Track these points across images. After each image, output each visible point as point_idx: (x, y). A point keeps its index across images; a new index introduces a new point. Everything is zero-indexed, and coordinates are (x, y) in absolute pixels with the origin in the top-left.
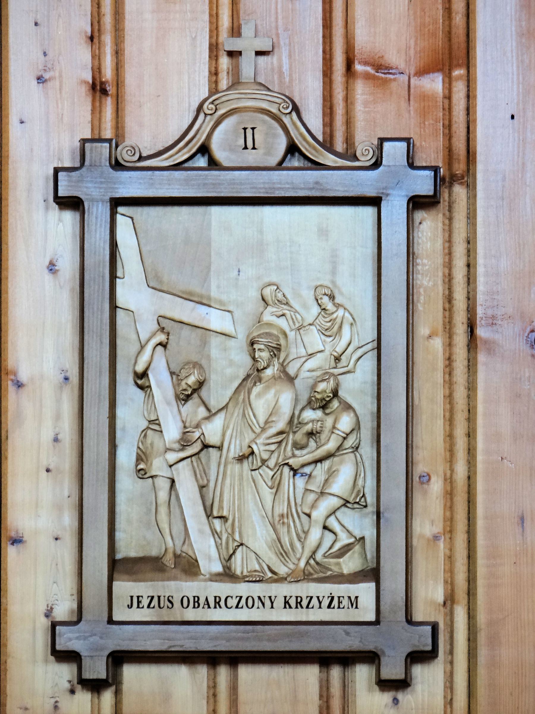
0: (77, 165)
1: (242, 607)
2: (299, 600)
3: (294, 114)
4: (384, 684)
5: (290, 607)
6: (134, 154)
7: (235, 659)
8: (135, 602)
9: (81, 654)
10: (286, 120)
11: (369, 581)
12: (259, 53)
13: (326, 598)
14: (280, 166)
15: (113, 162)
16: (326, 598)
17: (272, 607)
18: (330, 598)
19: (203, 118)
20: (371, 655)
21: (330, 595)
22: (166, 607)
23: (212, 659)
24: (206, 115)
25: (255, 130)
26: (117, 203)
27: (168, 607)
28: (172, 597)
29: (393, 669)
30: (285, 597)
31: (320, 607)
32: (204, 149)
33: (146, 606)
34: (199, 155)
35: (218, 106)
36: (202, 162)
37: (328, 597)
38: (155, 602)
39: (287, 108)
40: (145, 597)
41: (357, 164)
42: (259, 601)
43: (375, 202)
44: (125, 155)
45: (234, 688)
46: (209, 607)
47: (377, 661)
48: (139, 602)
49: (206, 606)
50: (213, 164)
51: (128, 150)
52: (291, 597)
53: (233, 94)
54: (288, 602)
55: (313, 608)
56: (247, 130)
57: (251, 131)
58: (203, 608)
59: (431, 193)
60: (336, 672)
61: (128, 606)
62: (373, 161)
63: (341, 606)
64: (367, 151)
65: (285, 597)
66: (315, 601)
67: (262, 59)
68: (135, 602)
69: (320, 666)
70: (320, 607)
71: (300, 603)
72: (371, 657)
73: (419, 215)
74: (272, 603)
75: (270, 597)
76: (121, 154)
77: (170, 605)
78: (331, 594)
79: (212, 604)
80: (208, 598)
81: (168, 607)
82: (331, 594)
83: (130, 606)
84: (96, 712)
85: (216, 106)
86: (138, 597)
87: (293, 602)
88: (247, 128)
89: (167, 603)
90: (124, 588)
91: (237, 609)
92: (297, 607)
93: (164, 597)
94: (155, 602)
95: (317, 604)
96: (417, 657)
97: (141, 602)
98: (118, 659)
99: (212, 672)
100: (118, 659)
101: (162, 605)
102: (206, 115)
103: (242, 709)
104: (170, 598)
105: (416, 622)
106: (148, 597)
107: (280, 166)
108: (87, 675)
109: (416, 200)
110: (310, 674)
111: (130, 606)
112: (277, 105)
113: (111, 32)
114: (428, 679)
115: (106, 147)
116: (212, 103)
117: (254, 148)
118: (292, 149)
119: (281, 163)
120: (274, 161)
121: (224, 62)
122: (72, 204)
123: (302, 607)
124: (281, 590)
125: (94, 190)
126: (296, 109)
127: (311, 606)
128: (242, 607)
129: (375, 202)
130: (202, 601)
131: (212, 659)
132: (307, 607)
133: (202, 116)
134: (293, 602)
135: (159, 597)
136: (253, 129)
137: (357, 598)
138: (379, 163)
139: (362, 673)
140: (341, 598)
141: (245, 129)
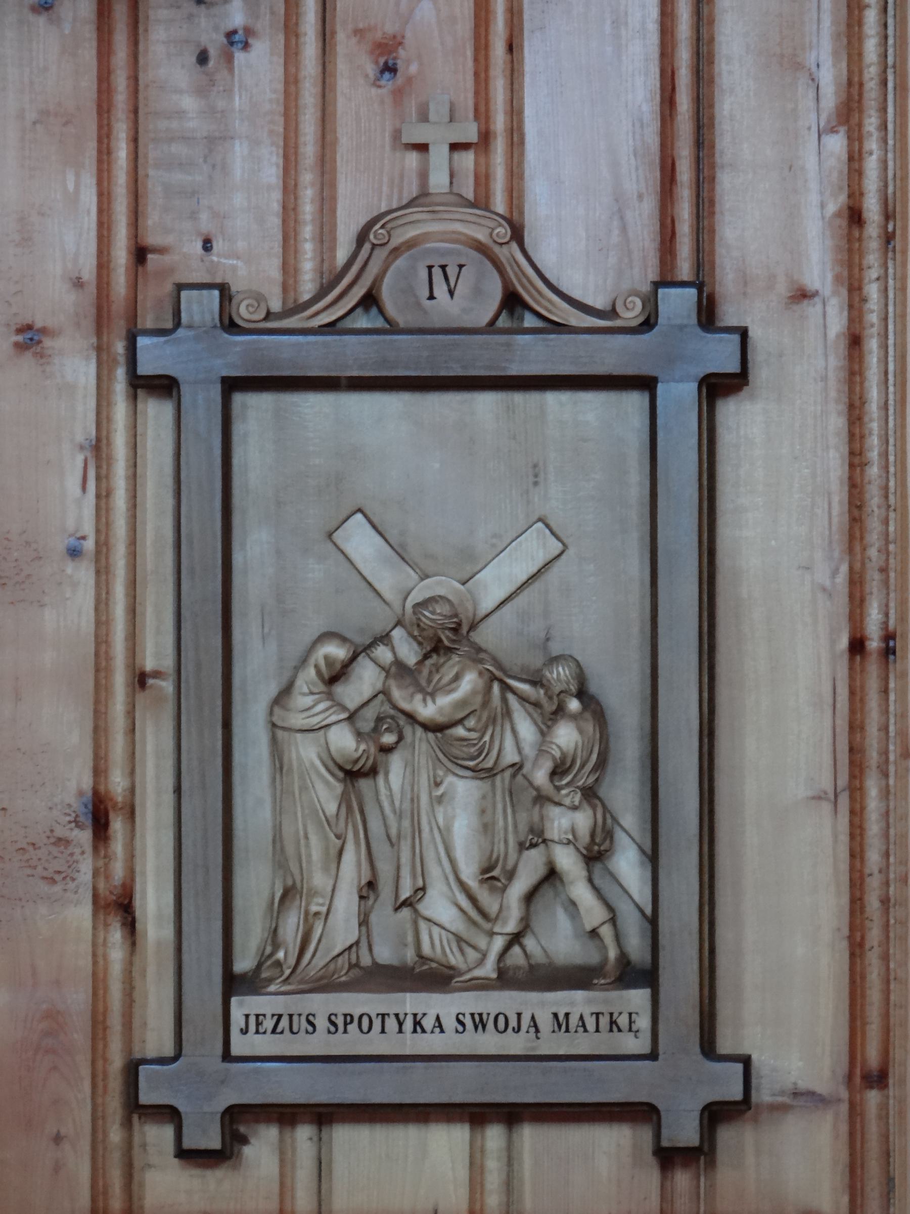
0: (169, 325)
1: (282, 1032)
2: (349, 1018)
3: (514, 246)
5: (424, 1031)
10: (502, 253)
15: (227, 321)
19: (369, 251)
20: (646, 1108)
23: (477, 1115)
25: (464, 269)
26: (232, 386)
29: (685, 1131)
32: (370, 301)
34: (359, 310)
38: (284, 1023)
39: (375, 237)
40: (269, 1016)
41: (618, 323)
43: (646, 384)
45: (322, 1169)
46: (586, 1031)
47: (655, 1118)
48: (258, 1024)
49: (581, 1029)
50: (393, 328)
51: (634, 303)
52: (620, 1013)
54: (615, 1023)
56: (433, 270)
58: (528, 1032)
60: (494, 1136)
61: (242, 1030)
63: (261, 1030)
64: (630, 306)
69: (472, 1129)
72: (641, 1113)
75: (397, 1015)
77: (310, 1029)
79: (591, 1026)
80: (536, 1017)
81: (307, 1032)
83: (244, 1031)
84: (303, 1198)
85: (388, 232)
86: (257, 1016)
88: (433, 266)
93: (300, 1015)
94: (284, 1023)
97: (261, 1023)
98: (238, 1120)
100: (238, 1120)
101: (295, 1029)
103: (340, 1199)
104: (311, 1018)
108: (188, 1143)
113: (879, 237)
116: (382, 227)
124: (321, 1004)
128: (282, 1032)
130: (526, 1021)
133: (367, 247)
134: (428, 1023)
135: (291, 1016)
137: (567, 1015)
140: (261, 1018)
141: (430, 268)
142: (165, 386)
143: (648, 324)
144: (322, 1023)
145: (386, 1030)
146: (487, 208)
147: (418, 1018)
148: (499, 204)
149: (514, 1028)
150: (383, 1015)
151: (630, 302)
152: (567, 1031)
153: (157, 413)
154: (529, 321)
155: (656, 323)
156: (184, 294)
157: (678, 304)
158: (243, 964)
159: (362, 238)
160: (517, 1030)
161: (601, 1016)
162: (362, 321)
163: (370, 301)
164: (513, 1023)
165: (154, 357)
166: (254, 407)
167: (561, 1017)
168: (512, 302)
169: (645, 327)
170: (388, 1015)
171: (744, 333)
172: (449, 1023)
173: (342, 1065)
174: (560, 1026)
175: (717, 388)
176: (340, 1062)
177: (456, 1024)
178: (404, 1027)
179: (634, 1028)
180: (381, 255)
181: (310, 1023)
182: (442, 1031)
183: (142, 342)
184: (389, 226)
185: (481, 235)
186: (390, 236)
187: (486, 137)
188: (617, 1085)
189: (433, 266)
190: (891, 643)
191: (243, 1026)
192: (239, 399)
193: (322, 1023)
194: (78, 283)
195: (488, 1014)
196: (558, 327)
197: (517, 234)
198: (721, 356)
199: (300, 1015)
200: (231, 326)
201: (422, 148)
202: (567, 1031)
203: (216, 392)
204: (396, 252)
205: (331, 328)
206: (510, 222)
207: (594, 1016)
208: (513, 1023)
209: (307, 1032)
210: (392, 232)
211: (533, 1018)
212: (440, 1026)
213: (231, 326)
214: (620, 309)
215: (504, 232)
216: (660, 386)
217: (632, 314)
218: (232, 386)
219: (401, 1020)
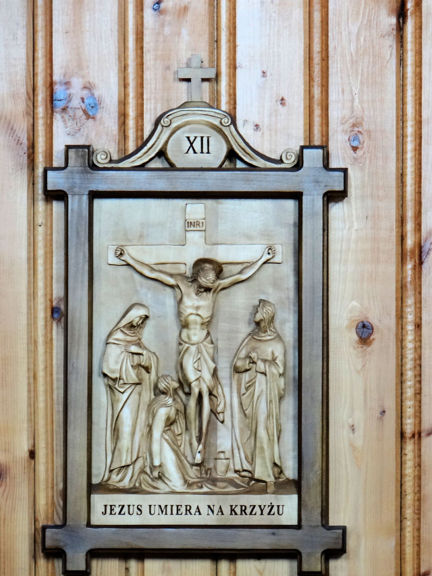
1: (124, 514)
2: (243, 508)
3: (232, 127)
5: (236, 514)
6: (106, 158)
8: (109, 509)
10: (226, 131)
11: (290, 493)
13: (266, 507)
14: (220, 169)
18: (270, 507)
24: (163, 126)
26: (95, 195)
27: (137, 514)
28: (141, 506)
30: (232, 506)
31: (262, 514)
32: (162, 154)
37: (269, 506)
38: (183, 510)
39: (228, 122)
40: (117, 506)
42: (209, 510)
43: (297, 196)
47: (299, 557)
48: (112, 510)
50: (172, 167)
52: (236, 506)
54: (234, 510)
55: (255, 514)
58: (217, 514)
59: (342, 188)
61: (103, 512)
62: (295, 163)
63: (113, 513)
64: (289, 157)
65: (232, 506)
66: (257, 509)
68: (109, 509)
70: (262, 514)
71: (189, 510)
76: (99, 163)
77: (139, 513)
78: (271, 503)
81: (137, 514)
82: (271, 503)
83: (105, 513)
85: (171, 121)
86: (178, 506)
89: (136, 510)
90: (99, 501)
92: (241, 514)
93: (134, 506)
94: (125, 509)
95: (259, 512)
97: (180, 510)
99: (140, 565)
101: (131, 513)
102: (163, 126)
104: (139, 507)
106: (119, 506)
111: (105, 513)
117: (208, 153)
119: (221, 166)
123: (246, 514)
127: (253, 513)
128: (124, 514)
129: (297, 196)
130: (216, 510)
132: (251, 514)
133: (159, 128)
135: (129, 506)
137: (166, 506)
138: (300, 165)
142: (59, 196)
143: (298, 165)
144: (145, 510)
146: (218, 108)
147: (233, 507)
148: (224, 106)
151: (290, 155)
152: (166, 514)
153: (57, 207)
154: (239, 165)
155: (302, 167)
156: (305, 151)
157: (313, 157)
158: (95, 481)
159: (157, 122)
162: (157, 164)
163: (162, 154)
165: (56, 181)
167: (163, 507)
168: (231, 155)
171: (345, 171)
172: (204, 510)
174: (162, 512)
175: (333, 197)
177: (141, 509)
181: (139, 509)
182: (200, 514)
183: (50, 174)
184: (170, 117)
185: (216, 122)
187: (218, 75)
188: (285, 541)
190: (140, 377)
191: (104, 511)
192: (97, 203)
193: (145, 510)
195: (166, 506)
196: (252, 168)
197: (234, 122)
199: (134, 506)
201: (188, 80)
202: (166, 514)
203: (85, 198)
205: (142, 167)
206: (230, 115)
210: (172, 120)
211: (220, 507)
214: (284, 159)
215: (227, 121)
216: (304, 198)
217: (290, 162)
218: (95, 195)
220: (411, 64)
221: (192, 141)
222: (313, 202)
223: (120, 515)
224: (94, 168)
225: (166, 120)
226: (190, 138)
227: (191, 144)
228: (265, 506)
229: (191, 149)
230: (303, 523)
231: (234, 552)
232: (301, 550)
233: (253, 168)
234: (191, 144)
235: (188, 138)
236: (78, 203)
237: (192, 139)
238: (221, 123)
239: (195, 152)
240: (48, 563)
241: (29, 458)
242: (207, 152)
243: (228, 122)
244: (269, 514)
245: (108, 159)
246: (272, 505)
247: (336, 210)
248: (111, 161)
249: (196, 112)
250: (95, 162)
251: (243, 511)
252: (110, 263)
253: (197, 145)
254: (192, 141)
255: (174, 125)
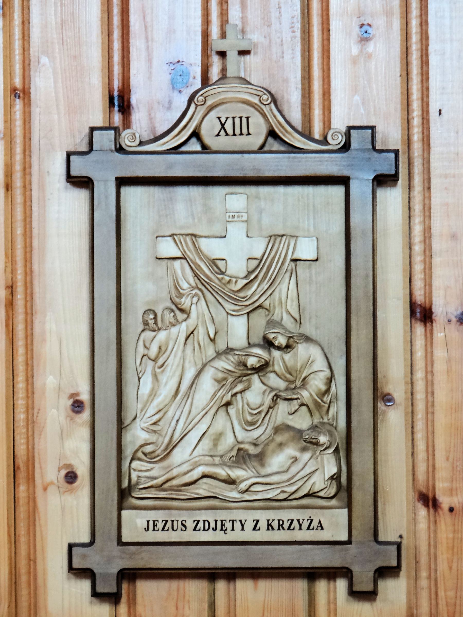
1: (168, 530)
2: (281, 522)
3: (272, 105)
4: (355, 594)
5: (273, 529)
7: (231, 575)
9: (95, 571)
10: (266, 109)
12: (243, 53)
13: (305, 521)
14: (261, 149)
15: (118, 146)
16: (305, 521)
17: (243, 529)
18: (309, 521)
21: (309, 518)
22: (179, 529)
23: (211, 575)
24: (197, 106)
26: (122, 182)
27: (182, 530)
28: (185, 521)
29: (364, 582)
30: (268, 521)
31: (300, 529)
32: (196, 134)
33: (161, 529)
35: (206, 98)
36: (195, 146)
37: (308, 520)
38: (201, 525)
39: (268, 100)
40: (228, 521)
43: (344, 181)
44: (126, 140)
48: (155, 526)
50: (205, 149)
52: (273, 520)
53: (219, 89)
57: (232, 119)
59: (393, 172)
60: (221, 586)
61: (145, 529)
63: (156, 529)
66: (295, 524)
67: (242, 58)
69: (308, 581)
70: (300, 529)
73: (380, 192)
74: (243, 526)
75: (241, 521)
77: (184, 529)
78: (310, 517)
82: (310, 517)
83: (147, 529)
85: (205, 98)
86: (154, 521)
87: (275, 524)
88: (235, 117)
91: (289, 531)
93: (177, 521)
94: (169, 525)
95: (297, 527)
96: (384, 572)
98: (129, 575)
100: (129, 575)
101: (175, 528)
104: (184, 522)
105: (382, 542)
106: (163, 521)
107: (261, 149)
109: (381, 178)
110: (301, 585)
111: (147, 529)
112: (258, 98)
114: (394, 590)
115: (111, 134)
116: (202, 95)
118: (272, 134)
120: (256, 148)
121: (216, 60)
122: (83, 183)
125: (103, 170)
126: (274, 100)
127: (292, 528)
128: (168, 530)
129: (344, 181)
131: (211, 575)
132: (289, 529)
133: (193, 106)
134: (275, 524)
135: (173, 521)
136: (247, 118)
139: (341, 585)
140: (224, 522)
143: (346, 147)
145: (235, 528)
149: (213, 528)
150: (233, 521)
160: (215, 529)
161: (235, 522)
163: (196, 134)
164: (213, 525)
165: (80, 167)
166: (128, 192)
169: (344, 150)
170: (236, 520)
172: (190, 525)
173: (179, 547)
176: (167, 546)
177: (186, 524)
178: (245, 527)
179: (224, 528)
180: (201, 111)
184: (205, 95)
185: (255, 100)
186: (205, 100)
189: (235, 117)
192: (126, 191)
194: (111, 141)
198: (385, 166)
199: (177, 521)
200: (120, 150)
204: (211, 108)
205: (175, 150)
207: (231, 522)
208: (213, 525)
209: (182, 530)
211: (320, 522)
212: (321, 526)
213: (120, 150)
216: (351, 181)
218: (122, 182)
219: (243, 523)
220: (118, 26)
221: (223, 123)
222: (361, 187)
223: (308, 531)
224: (122, 152)
225: (201, 98)
226: (221, 119)
227: (223, 125)
228: (303, 520)
229: (223, 131)
230: (353, 539)
231: (311, 571)
232: (352, 568)
233: (297, 150)
234: (223, 125)
235: (219, 118)
236: (105, 189)
237: (223, 120)
238: (260, 101)
239: (227, 134)
240: (329, 583)
241: (74, 470)
242: (240, 133)
243: (268, 100)
244: (308, 528)
245: (137, 142)
246: (311, 519)
247: (384, 194)
248: (141, 143)
249: (238, 89)
250: (124, 146)
251: (281, 526)
252: (158, 257)
253: (228, 126)
254: (223, 123)
255: (209, 103)
